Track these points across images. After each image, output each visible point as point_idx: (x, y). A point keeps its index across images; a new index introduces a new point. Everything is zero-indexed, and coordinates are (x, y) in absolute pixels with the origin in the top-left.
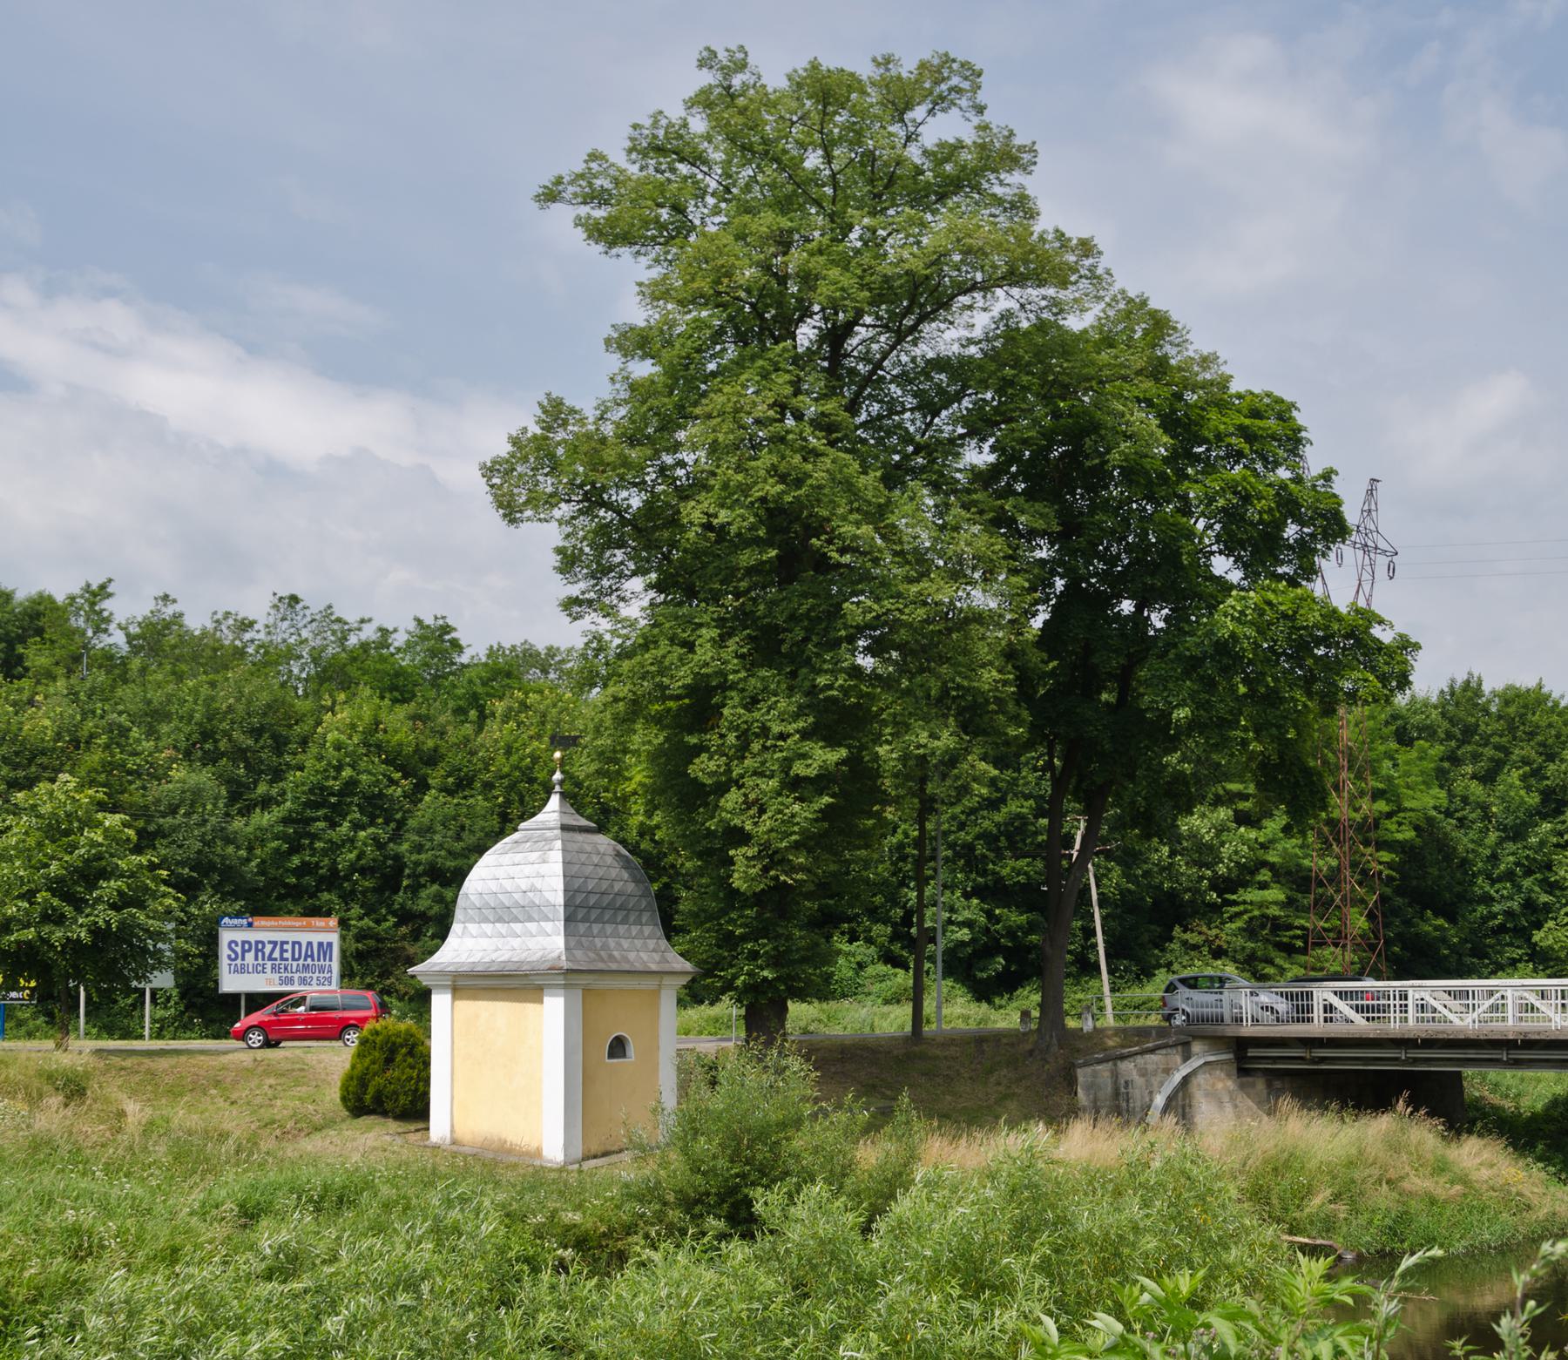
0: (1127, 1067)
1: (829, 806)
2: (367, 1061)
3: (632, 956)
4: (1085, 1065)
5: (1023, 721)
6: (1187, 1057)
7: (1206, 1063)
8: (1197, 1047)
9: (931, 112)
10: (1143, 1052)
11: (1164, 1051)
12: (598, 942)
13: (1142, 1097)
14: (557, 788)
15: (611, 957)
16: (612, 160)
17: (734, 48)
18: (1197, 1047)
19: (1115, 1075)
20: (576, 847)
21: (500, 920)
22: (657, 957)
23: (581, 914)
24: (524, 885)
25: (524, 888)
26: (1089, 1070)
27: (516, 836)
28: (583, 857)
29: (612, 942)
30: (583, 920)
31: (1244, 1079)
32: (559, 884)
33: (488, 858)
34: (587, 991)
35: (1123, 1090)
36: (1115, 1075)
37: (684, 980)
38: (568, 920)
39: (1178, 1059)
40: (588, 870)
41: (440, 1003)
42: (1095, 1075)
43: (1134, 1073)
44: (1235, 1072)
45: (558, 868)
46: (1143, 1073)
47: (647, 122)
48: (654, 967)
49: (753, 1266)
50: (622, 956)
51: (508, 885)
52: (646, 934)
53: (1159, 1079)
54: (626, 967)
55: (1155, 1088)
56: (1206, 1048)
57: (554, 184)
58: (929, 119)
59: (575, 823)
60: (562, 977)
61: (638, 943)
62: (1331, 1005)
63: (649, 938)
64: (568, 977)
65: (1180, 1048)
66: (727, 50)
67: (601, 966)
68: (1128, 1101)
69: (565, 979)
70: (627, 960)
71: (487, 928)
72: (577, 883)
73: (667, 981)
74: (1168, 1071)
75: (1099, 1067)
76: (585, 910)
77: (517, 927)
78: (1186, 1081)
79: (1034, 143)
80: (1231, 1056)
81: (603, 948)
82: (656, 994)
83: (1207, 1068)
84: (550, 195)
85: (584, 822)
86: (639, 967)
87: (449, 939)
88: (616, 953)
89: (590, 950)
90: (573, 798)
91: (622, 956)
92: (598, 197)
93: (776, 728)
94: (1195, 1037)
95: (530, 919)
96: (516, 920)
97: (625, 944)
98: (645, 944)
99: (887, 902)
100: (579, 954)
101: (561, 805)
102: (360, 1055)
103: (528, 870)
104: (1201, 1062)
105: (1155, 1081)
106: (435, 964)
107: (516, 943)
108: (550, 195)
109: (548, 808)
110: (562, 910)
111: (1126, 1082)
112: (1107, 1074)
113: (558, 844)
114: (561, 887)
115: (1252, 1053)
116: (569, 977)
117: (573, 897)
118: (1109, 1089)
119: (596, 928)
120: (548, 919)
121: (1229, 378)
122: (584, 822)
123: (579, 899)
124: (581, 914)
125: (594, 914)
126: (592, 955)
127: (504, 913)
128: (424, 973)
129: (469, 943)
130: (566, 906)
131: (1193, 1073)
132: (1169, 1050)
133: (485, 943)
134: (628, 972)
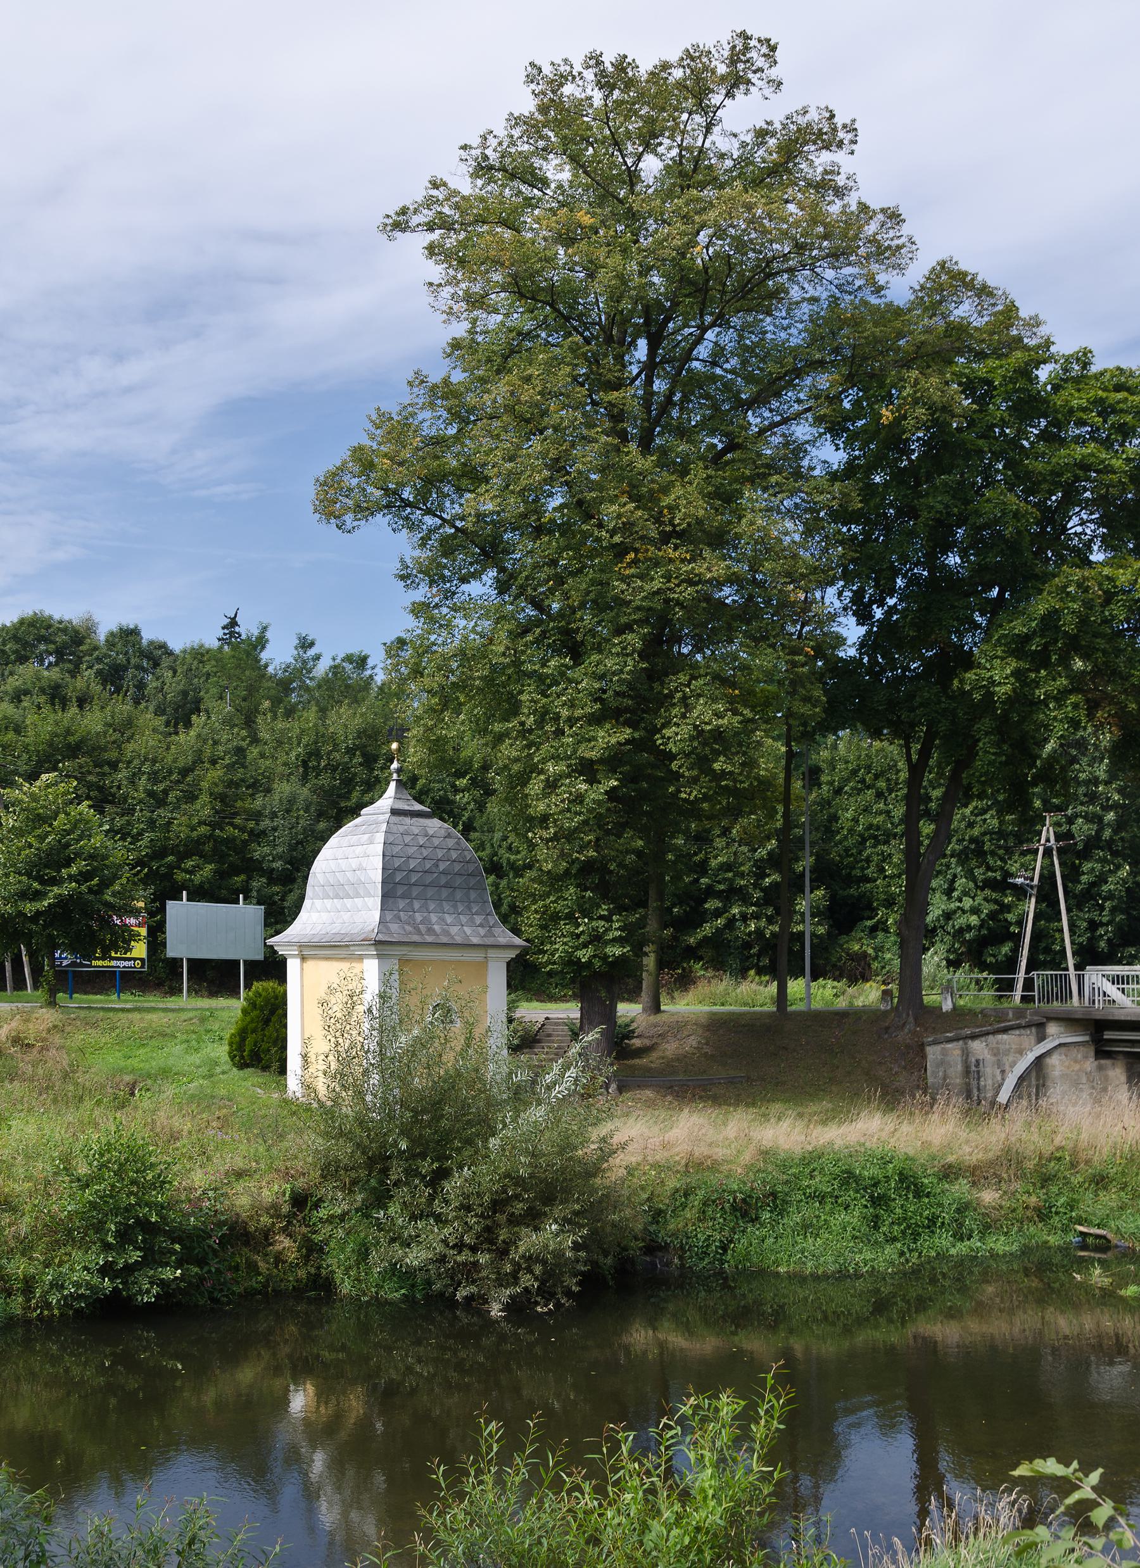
0: (978, 1047)
3: (454, 930)
4: (935, 1043)
5: (818, 700)
6: (1041, 1038)
7: (1060, 1045)
8: (1052, 1029)
9: (729, 95)
10: (995, 1032)
11: (1017, 1032)
12: (418, 917)
13: (994, 1076)
14: (395, 776)
15: (430, 931)
16: (452, 185)
17: (558, 61)
18: (1052, 1029)
19: (966, 1053)
20: (401, 829)
21: (337, 897)
22: (482, 931)
25: (354, 867)
26: (938, 1048)
27: (358, 820)
28: (407, 839)
29: (434, 918)
30: (403, 897)
31: (1103, 1062)
32: (378, 863)
33: (334, 840)
34: (403, 962)
35: (973, 1068)
36: (966, 1053)
37: (512, 954)
38: (385, 896)
39: (1033, 1039)
40: (411, 851)
42: (944, 1053)
43: (986, 1051)
44: (1092, 1054)
45: (379, 848)
46: (996, 1053)
47: (475, 141)
48: (475, 940)
50: (444, 930)
51: (343, 864)
52: (474, 911)
53: (1011, 1059)
54: (444, 940)
55: (1007, 1068)
56: (1062, 1029)
57: (398, 214)
58: (727, 102)
60: (373, 948)
61: (464, 919)
62: (1113, 983)
63: (476, 914)
64: (381, 946)
65: (1034, 1030)
66: (553, 64)
67: (416, 938)
68: (979, 1079)
70: (446, 933)
71: (328, 903)
72: (397, 863)
73: (492, 953)
74: (1021, 1052)
75: (949, 1046)
76: (406, 888)
77: (348, 902)
78: (1039, 1060)
79: (854, 121)
80: (1087, 1038)
81: (422, 922)
82: (483, 966)
83: (1063, 1050)
84: (399, 224)
85: (418, 807)
88: (436, 927)
90: (408, 783)
91: (444, 930)
92: (441, 223)
94: (1050, 1019)
95: (358, 896)
97: (449, 919)
98: (472, 920)
100: (394, 927)
101: (396, 793)
103: (359, 850)
104: (1056, 1043)
105: (1007, 1060)
106: (288, 936)
107: (346, 916)
108: (399, 224)
109: (386, 795)
110: (380, 886)
111: (977, 1061)
112: (958, 1052)
113: (384, 827)
114: (380, 866)
115: (1108, 1035)
116: (380, 947)
118: (960, 1067)
119: (417, 905)
120: (370, 896)
121: (516, 121)
122: (418, 807)
125: (415, 891)
126: (408, 928)
127: (340, 891)
129: (315, 916)
130: (384, 882)
131: (1049, 1053)
132: (1023, 1031)
133: (325, 917)
134: (445, 945)
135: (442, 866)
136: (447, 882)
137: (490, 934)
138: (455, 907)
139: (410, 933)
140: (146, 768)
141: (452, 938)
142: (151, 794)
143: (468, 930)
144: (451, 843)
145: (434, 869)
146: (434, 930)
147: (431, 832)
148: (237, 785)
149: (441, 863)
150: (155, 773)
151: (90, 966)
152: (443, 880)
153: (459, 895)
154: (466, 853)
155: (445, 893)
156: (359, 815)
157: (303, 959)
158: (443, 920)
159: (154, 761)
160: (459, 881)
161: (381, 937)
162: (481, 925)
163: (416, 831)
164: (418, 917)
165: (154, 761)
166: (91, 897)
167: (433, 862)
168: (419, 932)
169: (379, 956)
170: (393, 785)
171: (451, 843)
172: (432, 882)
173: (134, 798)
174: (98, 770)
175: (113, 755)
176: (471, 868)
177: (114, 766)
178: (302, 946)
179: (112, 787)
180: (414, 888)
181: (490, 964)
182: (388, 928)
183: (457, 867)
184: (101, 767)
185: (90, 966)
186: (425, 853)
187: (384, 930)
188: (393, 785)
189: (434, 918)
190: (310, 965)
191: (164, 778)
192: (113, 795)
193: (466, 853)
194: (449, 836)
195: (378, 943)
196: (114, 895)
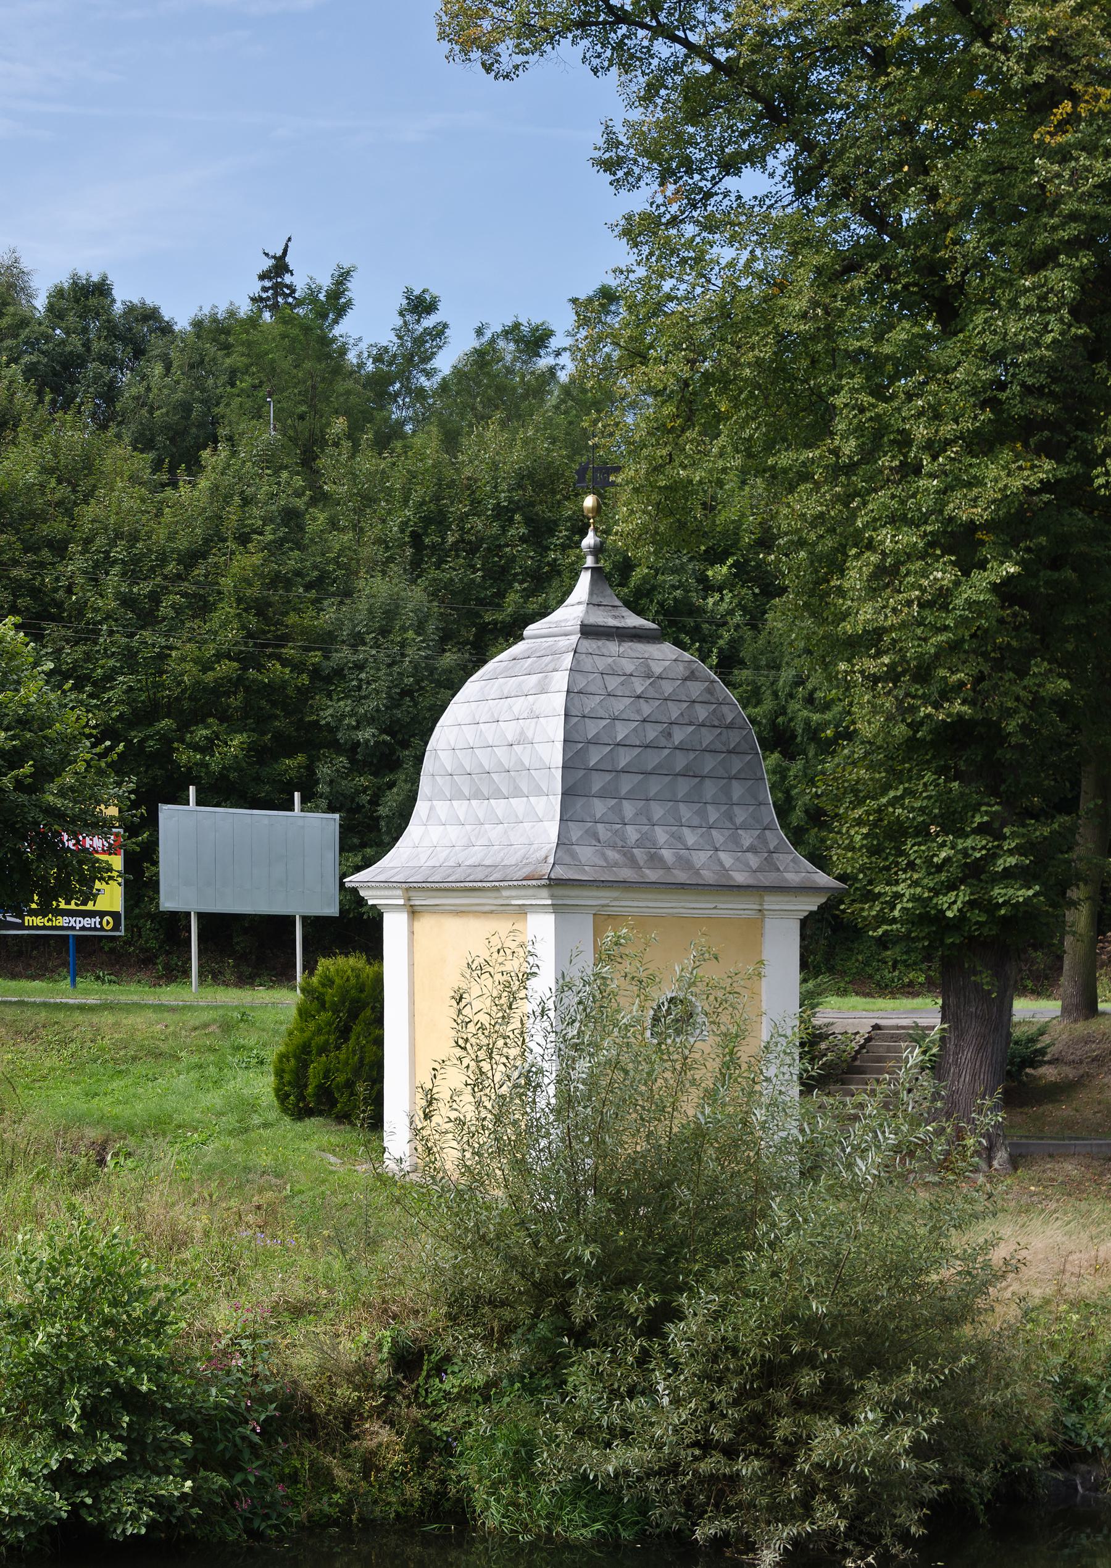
1: (1010, 578)
2: (312, 1026)
3: (700, 858)
14: (590, 561)
15: (655, 860)
20: (601, 663)
21: (477, 795)
22: (754, 861)
23: (598, 782)
24: (510, 731)
25: (510, 738)
28: (613, 683)
33: (472, 687)
34: (602, 919)
37: (812, 904)
38: (569, 793)
40: (620, 706)
41: (394, 927)
48: (740, 878)
49: (432, 1486)
50: (679, 858)
51: (490, 732)
54: (681, 876)
59: (612, 622)
60: (545, 892)
63: (745, 827)
67: (626, 874)
69: (552, 897)
73: (772, 902)
76: (608, 777)
77: (499, 806)
81: (639, 844)
82: (754, 928)
86: (709, 876)
87: (410, 828)
88: (667, 854)
89: (614, 847)
91: (679, 858)
93: (921, 431)
95: (517, 793)
96: (499, 795)
97: (691, 838)
99: (999, 722)
100: (586, 853)
101: (592, 593)
102: (304, 1014)
103: (519, 705)
107: (494, 833)
110: (558, 774)
113: (568, 660)
116: (559, 891)
117: (581, 754)
122: (633, 620)
123: (595, 756)
124: (598, 782)
125: (627, 784)
126: (612, 854)
128: (369, 885)
129: (435, 833)
134: (682, 886)
135: (679, 735)
136: (687, 767)
137: (769, 864)
138: (702, 814)
139: (616, 864)
140: (119, 552)
141: (697, 873)
142: (127, 601)
143: (726, 858)
144: (696, 689)
145: (663, 742)
146: (661, 859)
147: (657, 669)
148: (288, 584)
149: (675, 728)
150: (136, 560)
151: (21, 926)
152: (681, 761)
153: (710, 789)
154: (725, 709)
155: (683, 786)
156: (520, 638)
157: (414, 912)
158: (680, 838)
159: (134, 538)
160: (709, 763)
161: (560, 872)
162: (752, 849)
163: (629, 667)
164: (632, 834)
165: (134, 538)
166: (23, 798)
167: (660, 728)
168: (633, 862)
169: (557, 909)
170: (585, 579)
171: (696, 689)
172: (659, 766)
173: (96, 610)
174: (30, 557)
175: (57, 527)
176: (734, 737)
177: (59, 548)
178: (410, 888)
179: (56, 590)
180: (624, 776)
181: (768, 923)
182: (574, 855)
183: (708, 737)
184: (36, 550)
185: (21, 926)
186: (647, 709)
187: (567, 859)
188: (585, 579)
189: (661, 835)
190: (425, 924)
191: (152, 569)
192: (59, 605)
193: (725, 709)
194: (692, 676)
195: (554, 884)
196: (62, 793)
